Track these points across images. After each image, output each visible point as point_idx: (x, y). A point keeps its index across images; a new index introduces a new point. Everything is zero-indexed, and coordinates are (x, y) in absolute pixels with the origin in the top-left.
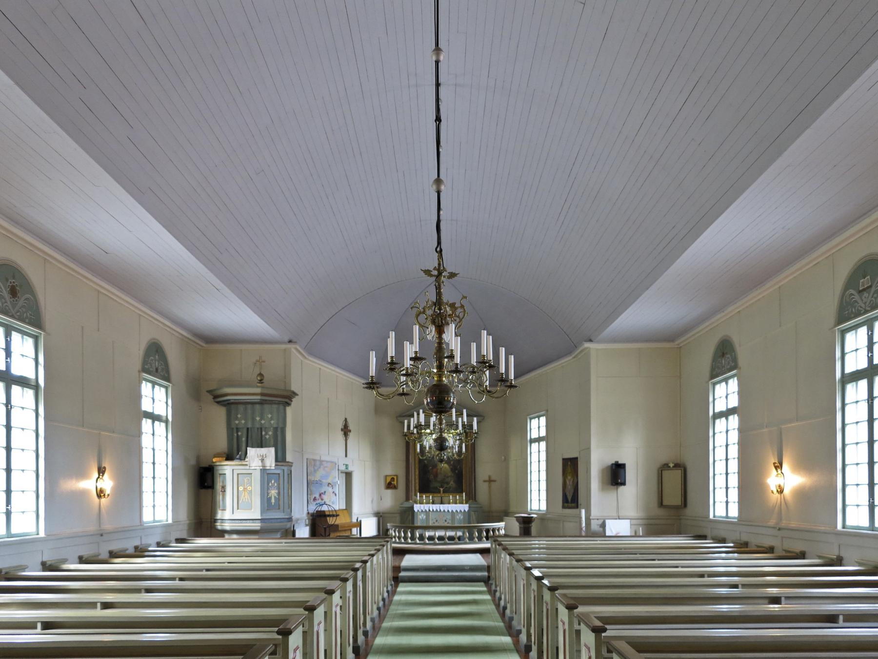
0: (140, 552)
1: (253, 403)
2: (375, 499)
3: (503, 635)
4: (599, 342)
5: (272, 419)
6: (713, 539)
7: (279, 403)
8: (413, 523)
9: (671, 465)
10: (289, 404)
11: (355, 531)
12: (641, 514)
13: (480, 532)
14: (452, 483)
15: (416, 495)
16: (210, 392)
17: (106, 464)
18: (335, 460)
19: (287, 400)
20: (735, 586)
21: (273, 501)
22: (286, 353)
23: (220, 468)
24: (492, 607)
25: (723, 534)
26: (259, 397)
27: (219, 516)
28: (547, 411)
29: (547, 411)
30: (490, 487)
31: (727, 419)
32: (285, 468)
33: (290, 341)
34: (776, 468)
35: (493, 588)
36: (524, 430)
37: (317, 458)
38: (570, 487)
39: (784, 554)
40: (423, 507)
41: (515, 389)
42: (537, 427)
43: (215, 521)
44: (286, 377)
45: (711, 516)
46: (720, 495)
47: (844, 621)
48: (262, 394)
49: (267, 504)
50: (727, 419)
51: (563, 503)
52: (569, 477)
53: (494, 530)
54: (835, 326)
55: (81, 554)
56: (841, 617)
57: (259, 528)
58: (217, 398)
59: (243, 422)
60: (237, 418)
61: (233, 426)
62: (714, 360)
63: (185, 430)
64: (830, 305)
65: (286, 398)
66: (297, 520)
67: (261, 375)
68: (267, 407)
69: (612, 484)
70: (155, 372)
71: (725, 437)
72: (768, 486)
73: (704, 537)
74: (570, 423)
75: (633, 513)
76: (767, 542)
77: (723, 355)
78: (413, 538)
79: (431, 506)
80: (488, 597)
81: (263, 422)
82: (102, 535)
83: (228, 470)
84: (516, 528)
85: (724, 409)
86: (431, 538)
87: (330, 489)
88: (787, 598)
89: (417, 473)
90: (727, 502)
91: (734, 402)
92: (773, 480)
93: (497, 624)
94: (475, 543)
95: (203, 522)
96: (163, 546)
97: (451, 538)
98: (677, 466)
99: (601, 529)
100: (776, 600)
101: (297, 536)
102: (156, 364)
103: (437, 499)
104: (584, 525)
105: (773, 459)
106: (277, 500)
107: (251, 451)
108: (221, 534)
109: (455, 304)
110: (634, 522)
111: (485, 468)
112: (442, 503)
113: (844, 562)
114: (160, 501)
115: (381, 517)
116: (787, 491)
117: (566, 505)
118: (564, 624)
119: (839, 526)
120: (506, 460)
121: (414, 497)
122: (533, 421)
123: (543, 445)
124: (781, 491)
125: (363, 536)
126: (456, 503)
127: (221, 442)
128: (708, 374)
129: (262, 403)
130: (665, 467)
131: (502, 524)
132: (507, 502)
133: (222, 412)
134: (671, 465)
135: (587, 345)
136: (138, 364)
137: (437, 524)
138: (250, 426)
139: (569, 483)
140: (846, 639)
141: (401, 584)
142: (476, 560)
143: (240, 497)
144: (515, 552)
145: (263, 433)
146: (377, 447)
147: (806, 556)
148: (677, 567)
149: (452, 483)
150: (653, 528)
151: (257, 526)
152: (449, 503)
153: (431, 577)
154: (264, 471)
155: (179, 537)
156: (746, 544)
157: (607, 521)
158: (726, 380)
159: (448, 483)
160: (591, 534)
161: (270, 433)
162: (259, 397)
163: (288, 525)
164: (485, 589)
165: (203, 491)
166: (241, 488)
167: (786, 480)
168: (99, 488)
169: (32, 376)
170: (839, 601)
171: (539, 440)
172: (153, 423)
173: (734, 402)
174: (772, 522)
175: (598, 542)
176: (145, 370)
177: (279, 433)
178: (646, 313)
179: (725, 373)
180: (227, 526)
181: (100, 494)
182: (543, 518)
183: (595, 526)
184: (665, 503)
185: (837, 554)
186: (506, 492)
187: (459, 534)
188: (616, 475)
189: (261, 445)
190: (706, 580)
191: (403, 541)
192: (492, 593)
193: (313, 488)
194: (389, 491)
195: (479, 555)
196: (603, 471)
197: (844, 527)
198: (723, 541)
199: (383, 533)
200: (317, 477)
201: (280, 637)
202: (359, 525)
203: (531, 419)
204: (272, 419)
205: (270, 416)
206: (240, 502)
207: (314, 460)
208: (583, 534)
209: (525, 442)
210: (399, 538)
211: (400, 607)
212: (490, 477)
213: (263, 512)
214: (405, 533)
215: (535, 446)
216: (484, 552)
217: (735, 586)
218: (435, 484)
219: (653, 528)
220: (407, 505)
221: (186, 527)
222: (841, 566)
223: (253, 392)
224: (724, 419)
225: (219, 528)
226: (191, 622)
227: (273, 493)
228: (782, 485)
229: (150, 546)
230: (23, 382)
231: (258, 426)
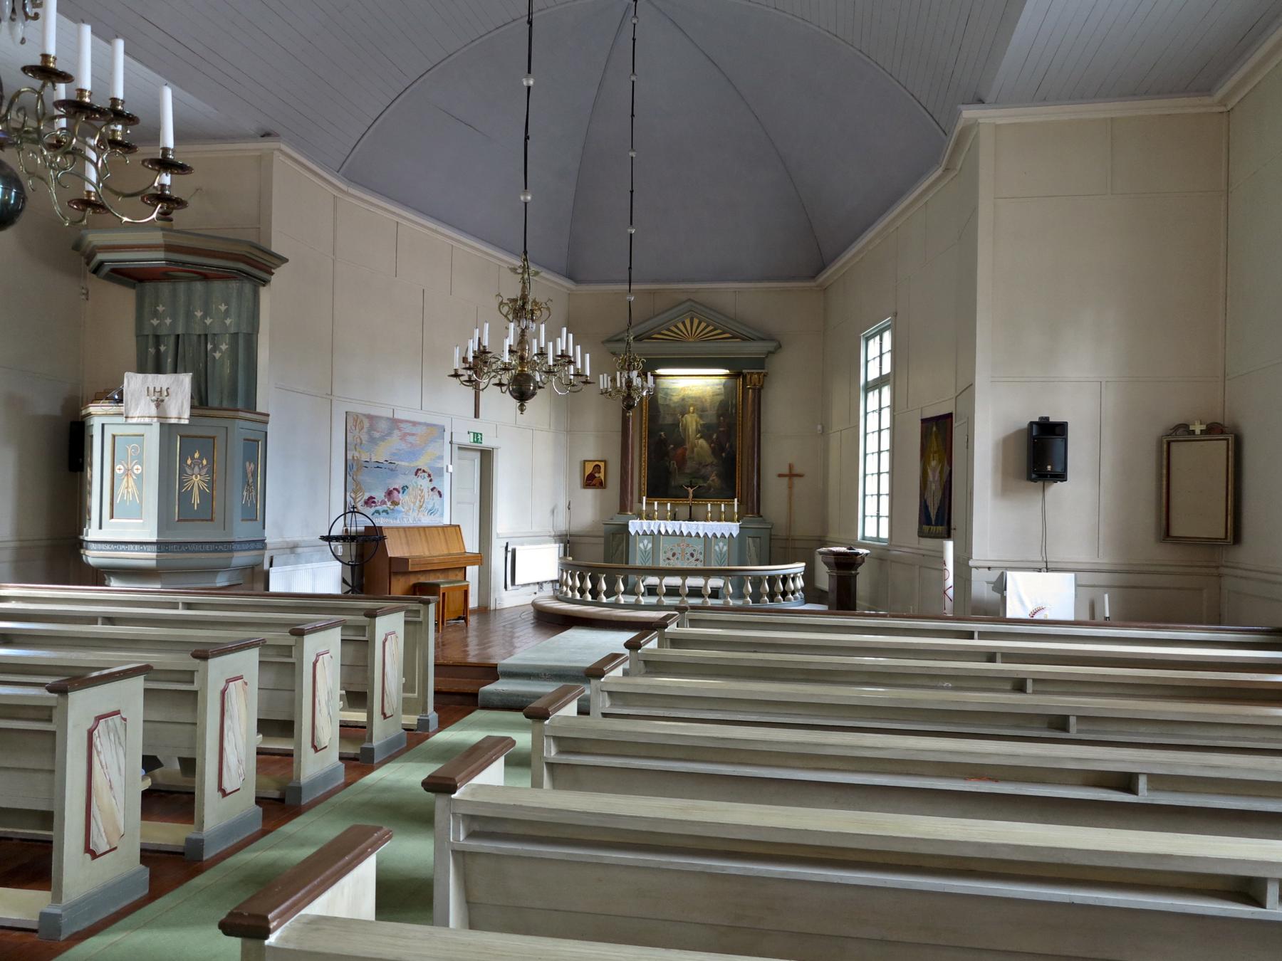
4: (998, 103)
9: (1198, 428)
10: (265, 282)
12: (1105, 560)
14: (713, 477)
21: (196, 500)
22: (263, 164)
26: (161, 255)
28: (895, 315)
29: (895, 315)
30: (790, 487)
33: (266, 135)
42: (876, 356)
48: (169, 248)
51: (921, 523)
52: (933, 463)
53: (785, 579)
57: (153, 563)
59: (168, 321)
60: (155, 314)
65: (252, 265)
68: (217, 286)
69: (1030, 479)
74: (941, 341)
75: (1083, 555)
81: (208, 321)
87: (424, 483)
89: (645, 456)
98: (1214, 430)
99: (999, 596)
103: (683, 510)
106: (207, 498)
107: (134, 383)
108: (97, 576)
110: (1086, 578)
111: (781, 447)
115: (570, 543)
117: (926, 528)
121: (636, 505)
123: (886, 391)
126: (719, 520)
130: (1181, 431)
131: (799, 567)
132: (824, 522)
134: (1198, 428)
135: (969, 113)
138: (180, 331)
139: (933, 477)
145: (209, 347)
149: (714, 480)
151: (148, 558)
152: (706, 520)
154: (168, 430)
157: (1011, 576)
159: (705, 478)
161: (224, 347)
166: (119, 469)
182: (883, 555)
183: (981, 587)
184: (1176, 531)
186: (821, 499)
188: (1041, 453)
191: (589, 598)
193: (364, 477)
194: (590, 493)
196: (1006, 443)
200: (381, 453)
203: (867, 340)
205: (223, 308)
206: (117, 501)
207: (371, 418)
209: (854, 388)
210: (572, 589)
212: (791, 467)
218: (681, 480)
220: (619, 520)
227: (197, 481)
231: (198, 330)
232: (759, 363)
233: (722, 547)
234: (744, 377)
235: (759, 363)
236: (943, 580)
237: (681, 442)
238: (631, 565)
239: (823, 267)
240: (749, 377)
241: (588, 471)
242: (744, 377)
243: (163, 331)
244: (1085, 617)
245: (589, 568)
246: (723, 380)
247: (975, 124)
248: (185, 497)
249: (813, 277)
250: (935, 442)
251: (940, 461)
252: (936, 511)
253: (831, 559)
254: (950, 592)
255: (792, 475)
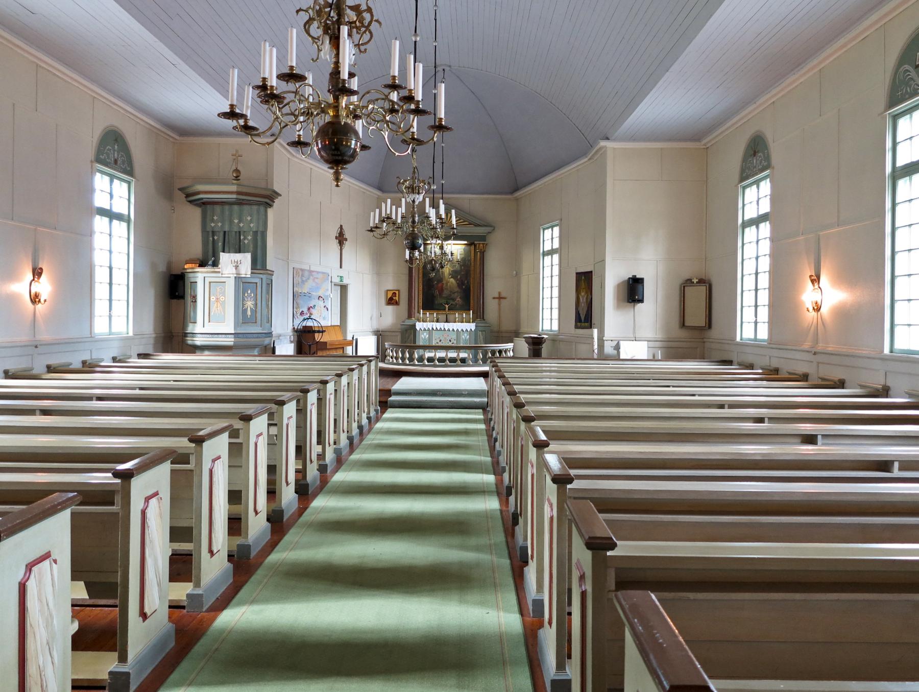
0: (88, 367)
1: (231, 204)
2: (375, 316)
3: (487, 473)
4: (615, 140)
5: (251, 221)
6: (739, 364)
7: (259, 204)
8: (415, 342)
9: (695, 281)
10: (271, 206)
11: (349, 350)
12: (659, 336)
13: (485, 354)
14: (458, 299)
15: (419, 312)
16: (180, 189)
17: (43, 265)
18: (328, 271)
19: (268, 201)
20: (760, 420)
21: (249, 313)
23: (191, 275)
24: (483, 440)
25: (750, 359)
26: (234, 196)
27: (190, 328)
30: (499, 305)
31: (757, 227)
32: (264, 277)
34: (813, 281)
35: (489, 416)
36: (536, 241)
37: (306, 267)
38: (583, 305)
39: (820, 382)
40: (428, 327)
41: (447, 134)
42: (550, 238)
43: (186, 335)
44: (268, 176)
45: (738, 339)
46: (748, 314)
47: (900, 469)
48: (238, 193)
49: (242, 317)
50: (757, 227)
54: (886, 110)
55: (7, 368)
56: (896, 465)
57: (232, 343)
58: (191, 197)
59: (220, 224)
60: (213, 221)
61: (209, 229)
62: (745, 160)
63: (151, 230)
64: (881, 93)
65: (267, 198)
66: (279, 336)
67: (237, 171)
68: (246, 208)
69: (628, 302)
70: (114, 164)
71: (755, 251)
72: (802, 303)
73: (730, 363)
74: (585, 231)
75: (650, 334)
76: (801, 369)
77: (755, 154)
78: (411, 359)
79: (434, 324)
80: (483, 426)
81: (241, 225)
82: (36, 347)
83: (201, 277)
84: (524, 348)
85: (755, 215)
86: (430, 360)
87: (321, 303)
88: (825, 436)
89: (421, 288)
90: (756, 323)
91: (765, 207)
92: (808, 295)
93: (483, 458)
94: (480, 366)
95: (172, 335)
96: (120, 361)
97: (453, 360)
98: (701, 281)
100: (810, 439)
101: (277, 353)
102: (114, 153)
104: (596, 346)
105: (809, 271)
106: (254, 312)
109: (359, 6)
110: (652, 344)
111: (495, 282)
112: (447, 321)
113: (891, 393)
114: (117, 309)
115: (380, 335)
116: (825, 310)
117: (579, 324)
118: (532, 466)
119: (887, 350)
120: (518, 275)
121: (417, 314)
122: (546, 231)
123: (556, 257)
124: (817, 309)
125: (359, 354)
127: (196, 248)
128: (737, 177)
129: (240, 203)
130: (688, 282)
131: (510, 346)
132: (518, 322)
133: (196, 213)
134: (695, 281)
135: (603, 143)
136: (90, 151)
137: (440, 344)
138: (227, 229)
139: (583, 300)
140: (909, 499)
141: (390, 410)
142: (478, 384)
143: (214, 309)
144: (507, 375)
146: (378, 259)
147: (846, 385)
148: (694, 395)
150: (673, 351)
151: (229, 341)
153: (420, 401)
154: (238, 279)
155: (142, 351)
156: (776, 371)
157: (622, 343)
158: (757, 183)
159: (454, 300)
160: (603, 357)
161: (249, 238)
162: (234, 196)
163: (267, 341)
164: (482, 417)
165: (174, 301)
166: (213, 298)
167: (825, 297)
168: (33, 292)
169: (126, 212)
170: (891, 442)
171: (551, 252)
172: (111, 222)
173: (765, 207)
174: (807, 346)
175: (611, 365)
176: (98, 160)
177: (259, 238)
178: (667, 104)
179: (757, 174)
180: (199, 341)
181: (35, 299)
182: (555, 339)
183: (609, 349)
184: (687, 324)
185: (883, 383)
186: (517, 310)
187: (463, 355)
188: (633, 290)
189: (239, 251)
190: (726, 412)
192: (487, 421)
193: (300, 302)
194: (390, 308)
195: (482, 379)
197: (891, 351)
198: (751, 367)
199: (381, 355)
201: (118, 481)
202: (355, 343)
203: (544, 230)
204: (251, 221)
205: (249, 218)
206: (212, 314)
207: (302, 270)
208: (595, 357)
210: (397, 358)
211: (379, 437)
212: (499, 293)
213: (236, 325)
214: (403, 353)
215: (548, 259)
216: (485, 375)
217: (760, 420)
218: (439, 301)
219: (673, 351)
220: (409, 322)
221: (152, 341)
222: (887, 397)
223: (227, 190)
224: (754, 228)
225: (190, 342)
226: (68, 454)
227: (250, 304)
228: (819, 302)
229: (102, 360)
230: (120, 217)
231: (236, 229)
232: (483, 238)
233: (466, 336)
234: (475, 246)
235: (483, 238)
236: (593, 345)
237: (440, 280)
238: (417, 344)
239: (517, 189)
240: (477, 245)
241: (389, 296)
242: (475, 246)
243: (216, 229)
244: (651, 358)
245: (407, 347)
246: (463, 247)
247: (605, 147)
248: (245, 311)
249: (512, 193)
250: (585, 283)
251: (586, 293)
252: (585, 316)
253: (531, 340)
254: (596, 351)
255: (500, 298)
